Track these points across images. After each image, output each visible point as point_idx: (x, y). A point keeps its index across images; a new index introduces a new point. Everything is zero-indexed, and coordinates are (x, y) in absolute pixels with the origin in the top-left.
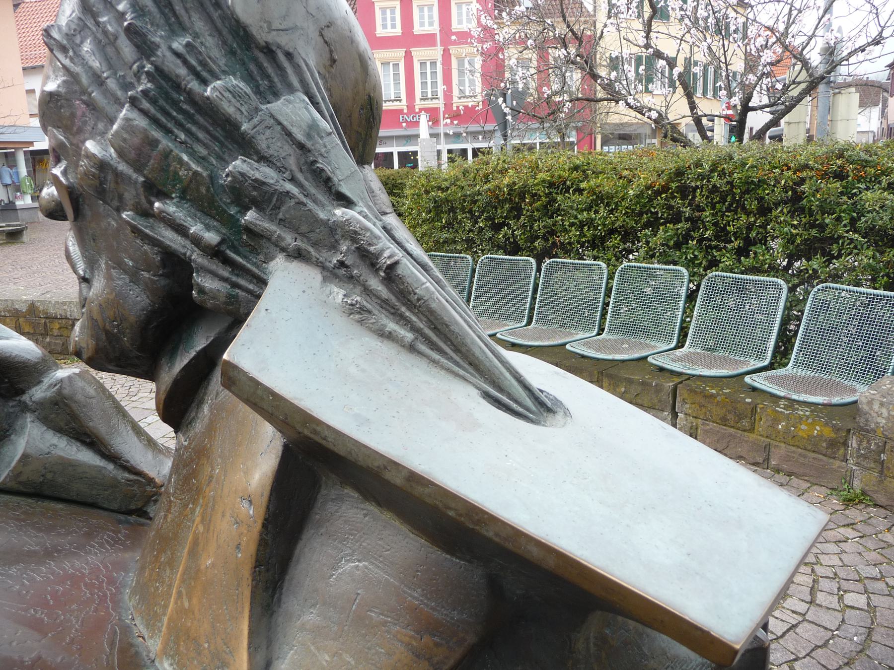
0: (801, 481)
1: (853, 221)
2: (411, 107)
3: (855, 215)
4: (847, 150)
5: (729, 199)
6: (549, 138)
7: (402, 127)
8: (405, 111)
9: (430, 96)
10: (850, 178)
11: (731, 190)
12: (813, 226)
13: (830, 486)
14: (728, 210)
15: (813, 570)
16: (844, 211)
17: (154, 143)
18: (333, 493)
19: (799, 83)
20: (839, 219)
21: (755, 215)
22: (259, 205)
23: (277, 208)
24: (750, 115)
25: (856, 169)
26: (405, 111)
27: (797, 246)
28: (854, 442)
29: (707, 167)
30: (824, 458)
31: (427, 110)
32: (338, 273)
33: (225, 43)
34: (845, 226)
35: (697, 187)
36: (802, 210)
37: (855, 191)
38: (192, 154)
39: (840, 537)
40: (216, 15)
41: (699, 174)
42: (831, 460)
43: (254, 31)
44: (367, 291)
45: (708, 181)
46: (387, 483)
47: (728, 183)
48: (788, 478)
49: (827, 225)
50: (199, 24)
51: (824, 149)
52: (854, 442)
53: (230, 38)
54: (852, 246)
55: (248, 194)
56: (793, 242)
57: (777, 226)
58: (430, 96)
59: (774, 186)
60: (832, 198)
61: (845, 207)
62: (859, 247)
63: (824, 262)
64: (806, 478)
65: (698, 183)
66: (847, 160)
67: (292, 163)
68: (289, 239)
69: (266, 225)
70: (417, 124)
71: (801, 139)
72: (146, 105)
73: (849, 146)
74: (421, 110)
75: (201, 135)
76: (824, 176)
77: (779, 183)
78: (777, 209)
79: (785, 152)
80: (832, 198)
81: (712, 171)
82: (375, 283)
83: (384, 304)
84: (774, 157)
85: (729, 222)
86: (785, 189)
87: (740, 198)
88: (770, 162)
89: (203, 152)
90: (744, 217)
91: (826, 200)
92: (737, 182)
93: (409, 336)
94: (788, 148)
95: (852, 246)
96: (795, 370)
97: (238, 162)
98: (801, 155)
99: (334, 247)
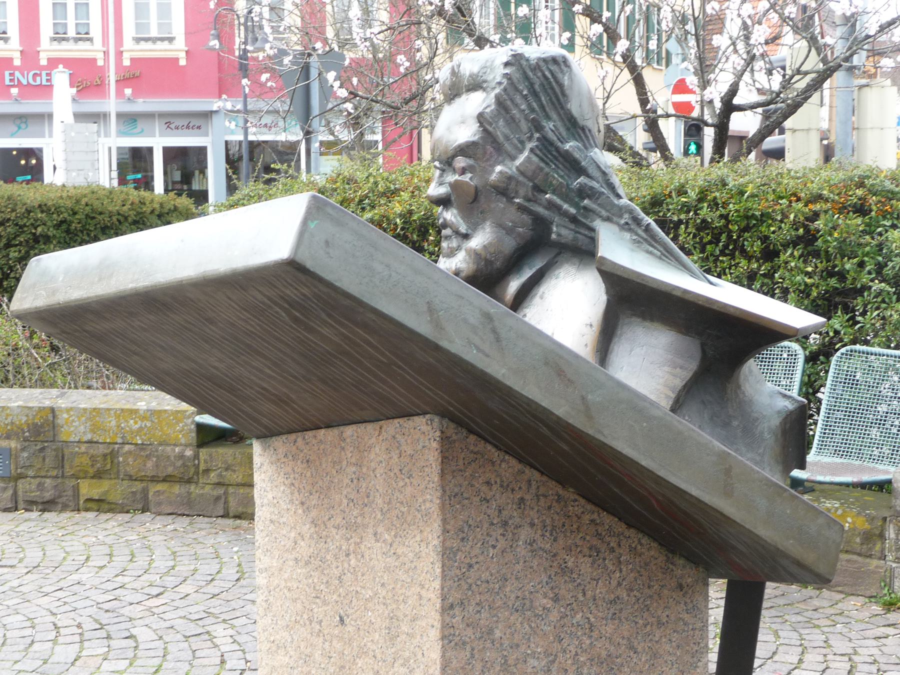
0: (833, 593)
1: (880, 267)
2: (30, 55)
3: (880, 259)
4: (868, 177)
5: (724, 238)
6: (332, 134)
7: (9, 96)
8: (17, 62)
9: (72, 33)
10: (873, 213)
11: (726, 226)
12: (831, 274)
13: (868, 593)
14: (722, 253)
15: (850, 660)
16: (867, 255)
17: (541, 169)
18: (627, 320)
19: (806, 73)
20: (861, 265)
21: (758, 261)
22: (589, 197)
23: (598, 198)
24: (735, 117)
25: (880, 201)
26: (17, 62)
27: (814, 301)
28: (892, 531)
29: (693, 195)
30: (860, 559)
31: (68, 63)
32: (626, 227)
33: (565, 125)
34: (869, 273)
35: (680, 222)
36: (816, 254)
37: (880, 229)
38: (558, 174)
39: (878, 634)
40: (562, 112)
41: (684, 205)
42: (868, 560)
43: (578, 120)
44: (637, 234)
45: (696, 214)
46: (674, 296)
47: (721, 216)
48: (818, 592)
49: (848, 271)
50: (554, 116)
51: (841, 175)
52: (892, 531)
53: (567, 123)
54: (879, 299)
55: (583, 192)
56: (808, 295)
57: (787, 274)
58: (72, 33)
59: (781, 221)
60: (853, 238)
61: (868, 249)
62: (887, 300)
63: (848, 321)
64: (840, 589)
65: (683, 216)
66: (869, 190)
67: (600, 179)
68: (604, 213)
69: (594, 206)
70: (46, 90)
71: (814, 156)
72: (538, 152)
73: (873, 172)
74: (53, 63)
75: (560, 166)
76: (843, 209)
77: (787, 217)
78: (786, 251)
79: (792, 178)
80: (853, 238)
81: (700, 200)
82: (640, 232)
83: (645, 240)
84: (780, 184)
85: (724, 269)
86: (795, 225)
87: (739, 237)
88: (774, 190)
89: (562, 174)
90: (743, 263)
91: (845, 240)
92: (733, 216)
93: (659, 253)
94: (796, 172)
95: (879, 299)
96: (819, 458)
97: (582, 178)
98: (812, 182)
99: (621, 216)
